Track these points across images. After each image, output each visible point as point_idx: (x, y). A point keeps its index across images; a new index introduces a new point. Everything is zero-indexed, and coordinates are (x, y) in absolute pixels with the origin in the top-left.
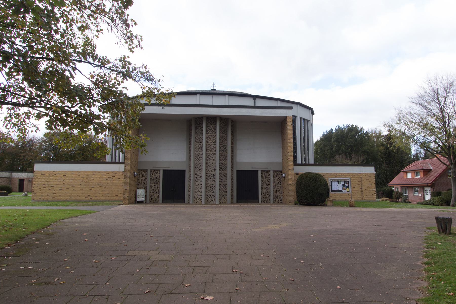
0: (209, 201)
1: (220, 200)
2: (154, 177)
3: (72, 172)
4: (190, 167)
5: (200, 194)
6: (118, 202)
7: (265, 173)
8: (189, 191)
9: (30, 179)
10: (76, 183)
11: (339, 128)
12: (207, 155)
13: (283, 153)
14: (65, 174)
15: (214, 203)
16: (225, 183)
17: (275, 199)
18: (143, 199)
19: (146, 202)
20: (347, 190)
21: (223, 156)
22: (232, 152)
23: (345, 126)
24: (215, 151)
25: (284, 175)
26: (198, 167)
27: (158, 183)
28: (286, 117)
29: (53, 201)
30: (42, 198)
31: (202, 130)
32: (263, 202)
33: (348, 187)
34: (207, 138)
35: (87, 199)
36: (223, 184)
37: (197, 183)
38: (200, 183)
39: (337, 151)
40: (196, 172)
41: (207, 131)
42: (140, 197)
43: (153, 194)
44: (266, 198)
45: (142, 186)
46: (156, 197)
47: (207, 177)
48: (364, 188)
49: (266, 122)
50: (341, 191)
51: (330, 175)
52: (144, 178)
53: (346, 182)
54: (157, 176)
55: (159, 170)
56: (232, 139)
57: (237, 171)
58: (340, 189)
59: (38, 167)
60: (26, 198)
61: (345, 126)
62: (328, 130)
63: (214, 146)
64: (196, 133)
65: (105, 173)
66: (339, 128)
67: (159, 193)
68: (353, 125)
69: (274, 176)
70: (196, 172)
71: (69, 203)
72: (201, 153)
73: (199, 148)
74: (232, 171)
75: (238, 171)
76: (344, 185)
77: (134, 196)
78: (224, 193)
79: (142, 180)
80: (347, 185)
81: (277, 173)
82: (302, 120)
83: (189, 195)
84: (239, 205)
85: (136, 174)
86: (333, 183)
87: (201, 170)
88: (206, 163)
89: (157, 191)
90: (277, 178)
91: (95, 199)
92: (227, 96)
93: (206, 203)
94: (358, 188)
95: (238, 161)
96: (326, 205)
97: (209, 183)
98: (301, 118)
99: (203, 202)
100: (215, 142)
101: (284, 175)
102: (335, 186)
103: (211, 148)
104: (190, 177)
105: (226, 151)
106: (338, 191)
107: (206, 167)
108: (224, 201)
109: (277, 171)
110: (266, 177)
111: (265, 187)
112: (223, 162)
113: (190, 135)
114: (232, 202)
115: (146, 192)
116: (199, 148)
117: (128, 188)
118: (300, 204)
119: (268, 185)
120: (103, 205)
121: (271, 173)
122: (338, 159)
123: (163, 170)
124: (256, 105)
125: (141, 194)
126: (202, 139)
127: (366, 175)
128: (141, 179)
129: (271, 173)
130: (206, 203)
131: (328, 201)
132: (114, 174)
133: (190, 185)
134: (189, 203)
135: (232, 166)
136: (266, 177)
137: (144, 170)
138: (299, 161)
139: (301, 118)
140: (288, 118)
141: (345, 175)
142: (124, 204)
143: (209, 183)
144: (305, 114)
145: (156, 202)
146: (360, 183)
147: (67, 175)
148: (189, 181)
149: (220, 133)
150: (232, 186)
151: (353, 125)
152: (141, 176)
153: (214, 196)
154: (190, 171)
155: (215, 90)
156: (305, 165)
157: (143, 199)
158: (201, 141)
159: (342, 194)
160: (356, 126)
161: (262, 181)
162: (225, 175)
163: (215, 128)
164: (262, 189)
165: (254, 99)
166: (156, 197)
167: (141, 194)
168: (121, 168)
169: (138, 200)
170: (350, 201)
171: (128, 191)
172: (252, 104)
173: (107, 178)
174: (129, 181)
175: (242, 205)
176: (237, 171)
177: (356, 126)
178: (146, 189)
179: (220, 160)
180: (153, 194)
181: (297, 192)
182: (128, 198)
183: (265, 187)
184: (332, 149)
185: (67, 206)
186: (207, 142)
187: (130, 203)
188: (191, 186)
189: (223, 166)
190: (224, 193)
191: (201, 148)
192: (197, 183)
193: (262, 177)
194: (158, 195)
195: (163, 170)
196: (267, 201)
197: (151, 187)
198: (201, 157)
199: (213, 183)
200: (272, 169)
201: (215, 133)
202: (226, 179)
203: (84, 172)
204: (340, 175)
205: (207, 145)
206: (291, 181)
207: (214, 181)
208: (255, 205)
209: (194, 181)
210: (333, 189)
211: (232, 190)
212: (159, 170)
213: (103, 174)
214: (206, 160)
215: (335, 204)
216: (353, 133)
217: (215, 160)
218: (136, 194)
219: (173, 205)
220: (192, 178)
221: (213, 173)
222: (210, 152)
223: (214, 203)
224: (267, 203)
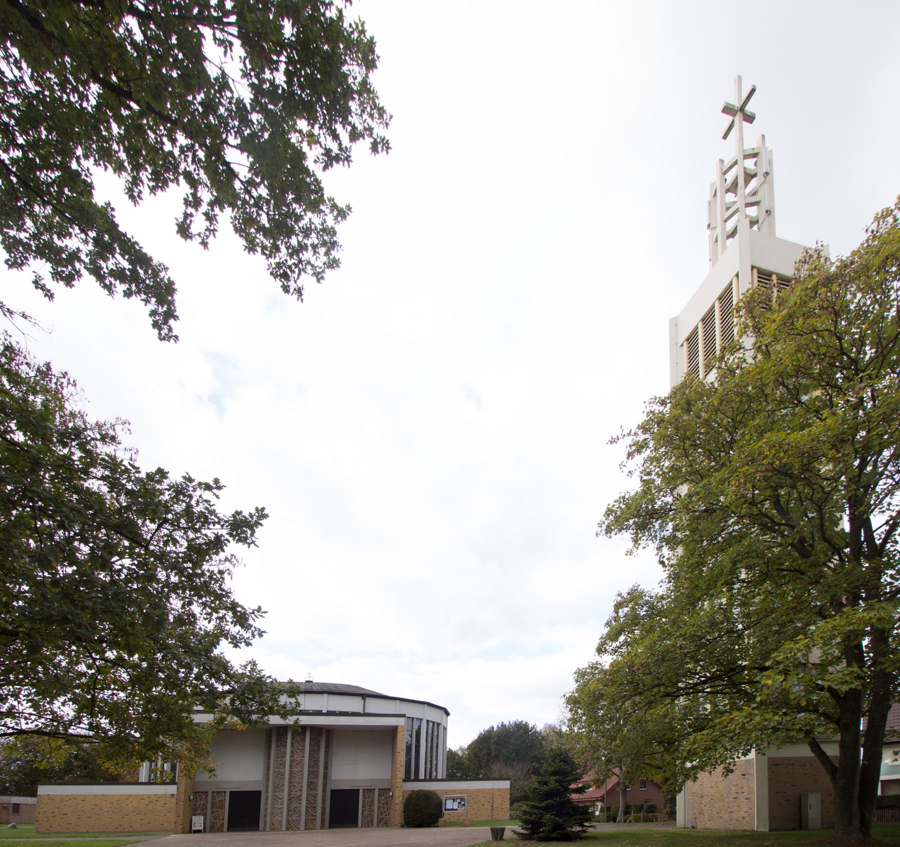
0: (291, 826)
1: (306, 825)
2: (218, 801)
3: (96, 796)
4: (267, 787)
5: (280, 819)
6: (167, 832)
7: (370, 791)
8: (265, 816)
9: (6, 805)
10: (101, 809)
11: (503, 725)
12: (291, 772)
13: (392, 768)
14: (84, 799)
15: (299, 829)
16: (314, 805)
17: (379, 822)
18: (202, 828)
19: (205, 832)
20: (463, 808)
21: (313, 772)
22: (326, 768)
23: (512, 723)
24: (303, 767)
25: (391, 794)
26: (278, 787)
27: (222, 807)
28: (397, 726)
29: (68, 833)
30: (51, 829)
31: (286, 742)
32: (363, 826)
33: (464, 805)
34: (292, 752)
35: (118, 830)
36: (311, 805)
37: (277, 807)
38: (281, 806)
39: (497, 757)
40: (276, 794)
41: (292, 744)
42: (197, 825)
43: (215, 821)
44: (368, 821)
45: (199, 811)
46: (219, 824)
47: (290, 800)
48: (495, 806)
49: (373, 731)
50: (456, 810)
51: (446, 792)
52: (202, 802)
53: (462, 799)
54: (221, 799)
55: (225, 792)
56: (327, 753)
57: (332, 791)
58: (456, 807)
59: (42, 790)
60: (14, 830)
61: (512, 723)
62: (487, 728)
63: (302, 761)
64: (278, 746)
65: (143, 797)
66: (503, 725)
67: (223, 820)
68: (522, 721)
69: (380, 795)
70: (276, 794)
71: (97, 835)
72: (283, 770)
73: (281, 765)
74: (324, 791)
75: (333, 791)
76: (459, 803)
77: (188, 824)
78: (312, 818)
79: (200, 805)
80: (463, 803)
81: (384, 791)
82: (431, 724)
83: (265, 821)
84: (330, 830)
85: (192, 797)
86: (447, 801)
87: (283, 790)
88: (290, 783)
89: (221, 817)
90: (383, 797)
91: (131, 829)
92: (325, 696)
93: (288, 829)
94: (488, 806)
95: (333, 778)
96: (438, 826)
97: (293, 806)
98: (428, 721)
99: (284, 828)
100: (303, 757)
101: (391, 794)
102: (450, 804)
103: (297, 764)
104: (267, 799)
105: (318, 767)
106: (452, 809)
107: (290, 787)
108: (311, 827)
109: (384, 789)
110: (369, 797)
111: (368, 808)
112: (313, 780)
113: (270, 748)
114: (322, 827)
115: (205, 819)
116: (281, 765)
117: (181, 815)
118: (408, 827)
119: (372, 805)
120: (145, 835)
121: (377, 792)
122: (496, 767)
123: (231, 792)
124: (367, 711)
125: (198, 822)
126: (285, 753)
127: (499, 790)
128: (198, 803)
129: (377, 792)
130: (288, 829)
131: (441, 820)
132: (158, 798)
133: (266, 809)
134: (264, 830)
135: (325, 785)
136: (369, 797)
137: (202, 792)
138: (422, 776)
139: (428, 721)
140: (399, 729)
141: (461, 791)
142: (175, 833)
143: (293, 806)
144: (435, 716)
145: (220, 830)
146: (490, 800)
147: (87, 799)
148: (266, 804)
149: (310, 746)
150: (324, 808)
151: (522, 721)
152: (198, 800)
153: (298, 821)
154: (267, 792)
155: (311, 682)
156: (431, 780)
157: (202, 828)
158: (284, 756)
159: (459, 813)
160: (526, 723)
161: (364, 801)
162: (315, 796)
163: (304, 740)
164: (363, 811)
165: (364, 699)
166: (219, 824)
167: (198, 822)
168: (172, 789)
169: (193, 828)
170: (464, 820)
171: (181, 818)
172: (369, 701)
173: (147, 803)
174: (182, 807)
175: (334, 830)
176: (332, 791)
177: (526, 723)
178: (205, 815)
179: (308, 778)
180: (215, 821)
181: (404, 812)
182: (181, 827)
183: (368, 808)
184: (490, 754)
185: (96, 837)
186: (292, 757)
187: (183, 833)
188: (269, 810)
189: (312, 785)
190: (312, 818)
191: (284, 765)
192: (277, 807)
193: (364, 797)
194: (222, 822)
195: (231, 792)
196: (368, 824)
197: (212, 812)
198: (283, 775)
199: (297, 805)
200: (377, 787)
201: (304, 746)
202: (315, 801)
203: (114, 796)
204: (455, 791)
205: (291, 761)
206: (398, 800)
207: (300, 803)
208: (355, 829)
209: (273, 804)
210: (447, 808)
211: (323, 813)
212: (225, 792)
213: (142, 798)
214: (290, 778)
215: (446, 824)
216: (521, 731)
217: (302, 779)
218: (191, 822)
219: (243, 833)
220: (269, 801)
221: (299, 794)
222: (295, 769)
223: (299, 829)
224: (369, 826)
